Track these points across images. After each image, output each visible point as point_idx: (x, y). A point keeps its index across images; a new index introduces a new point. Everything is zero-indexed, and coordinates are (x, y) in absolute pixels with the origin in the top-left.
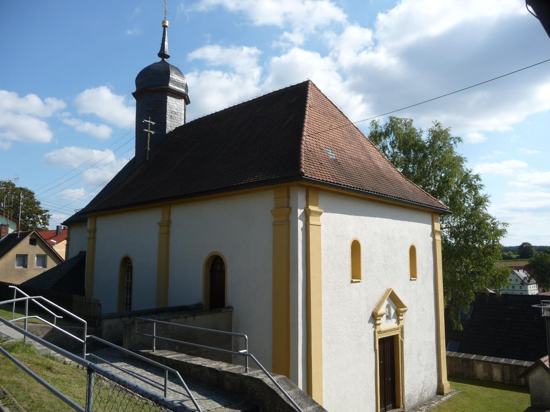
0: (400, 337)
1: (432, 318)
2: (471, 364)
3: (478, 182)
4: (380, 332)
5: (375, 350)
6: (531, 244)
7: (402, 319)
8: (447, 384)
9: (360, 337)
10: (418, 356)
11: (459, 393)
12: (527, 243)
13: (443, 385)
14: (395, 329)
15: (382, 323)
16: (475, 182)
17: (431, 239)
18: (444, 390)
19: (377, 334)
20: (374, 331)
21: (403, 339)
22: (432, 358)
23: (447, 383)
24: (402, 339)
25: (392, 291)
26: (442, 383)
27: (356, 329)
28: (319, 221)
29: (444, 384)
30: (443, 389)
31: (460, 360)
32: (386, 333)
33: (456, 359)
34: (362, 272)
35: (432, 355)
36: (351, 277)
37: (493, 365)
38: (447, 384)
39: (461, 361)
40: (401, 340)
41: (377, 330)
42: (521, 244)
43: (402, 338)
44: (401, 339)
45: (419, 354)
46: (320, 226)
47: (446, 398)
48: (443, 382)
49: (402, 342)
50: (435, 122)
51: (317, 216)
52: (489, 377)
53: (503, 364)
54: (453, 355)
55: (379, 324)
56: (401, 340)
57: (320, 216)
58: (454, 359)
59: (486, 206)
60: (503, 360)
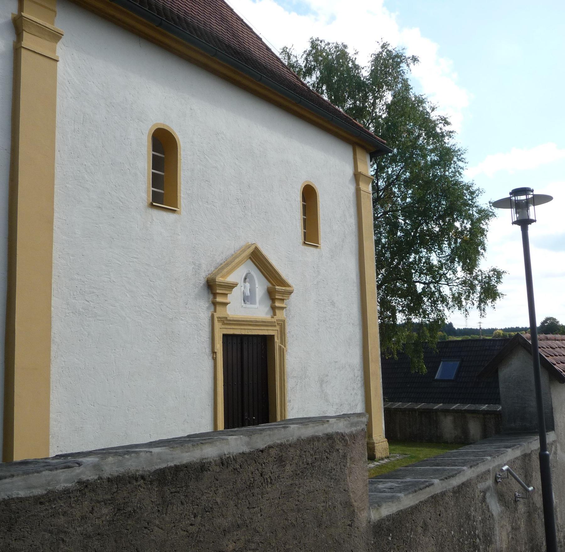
0: (277, 340)
1: (353, 324)
2: (435, 418)
3: (447, 128)
4: (225, 321)
5: (214, 353)
6: (556, 319)
7: (282, 308)
8: (384, 442)
9: (171, 320)
10: (321, 386)
11: (404, 458)
12: (552, 318)
13: (374, 443)
14: (264, 324)
15: (230, 303)
16: (441, 129)
17: (352, 189)
18: (376, 451)
19: (217, 325)
20: (210, 315)
21: (285, 347)
22: (353, 394)
23: (382, 440)
24: (283, 346)
25: (256, 248)
26: (373, 440)
27: (160, 301)
28: (54, 51)
29: (375, 441)
30: (375, 450)
31: (417, 412)
32: (242, 327)
33: (410, 413)
34: (182, 195)
35: (354, 389)
36: (148, 196)
37: (468, 415)
38: (384, 442)
39: (419, 415)
40: (280, 347)
41: (216, 315)
42: (544, 320)
43: (282, 343)
44: (280, 345)
45: (322, 381)
46: (57, 61)
47: (378, 464)
48: (373, 438)
49: (282, 352)
50: (380, 41)
51: (46, 39)
52: (463, 437)
53: (486, 413)
54: (406, 406)
55: (225, 304)
56: (280, 347)
57: (57, 43)
58: (407, 412)
59: (459, 169)
60: (484, 407)
